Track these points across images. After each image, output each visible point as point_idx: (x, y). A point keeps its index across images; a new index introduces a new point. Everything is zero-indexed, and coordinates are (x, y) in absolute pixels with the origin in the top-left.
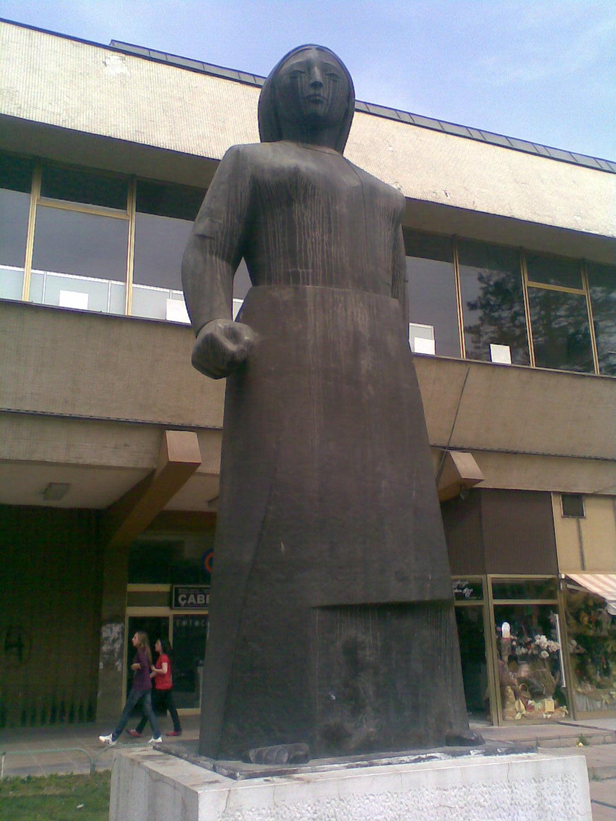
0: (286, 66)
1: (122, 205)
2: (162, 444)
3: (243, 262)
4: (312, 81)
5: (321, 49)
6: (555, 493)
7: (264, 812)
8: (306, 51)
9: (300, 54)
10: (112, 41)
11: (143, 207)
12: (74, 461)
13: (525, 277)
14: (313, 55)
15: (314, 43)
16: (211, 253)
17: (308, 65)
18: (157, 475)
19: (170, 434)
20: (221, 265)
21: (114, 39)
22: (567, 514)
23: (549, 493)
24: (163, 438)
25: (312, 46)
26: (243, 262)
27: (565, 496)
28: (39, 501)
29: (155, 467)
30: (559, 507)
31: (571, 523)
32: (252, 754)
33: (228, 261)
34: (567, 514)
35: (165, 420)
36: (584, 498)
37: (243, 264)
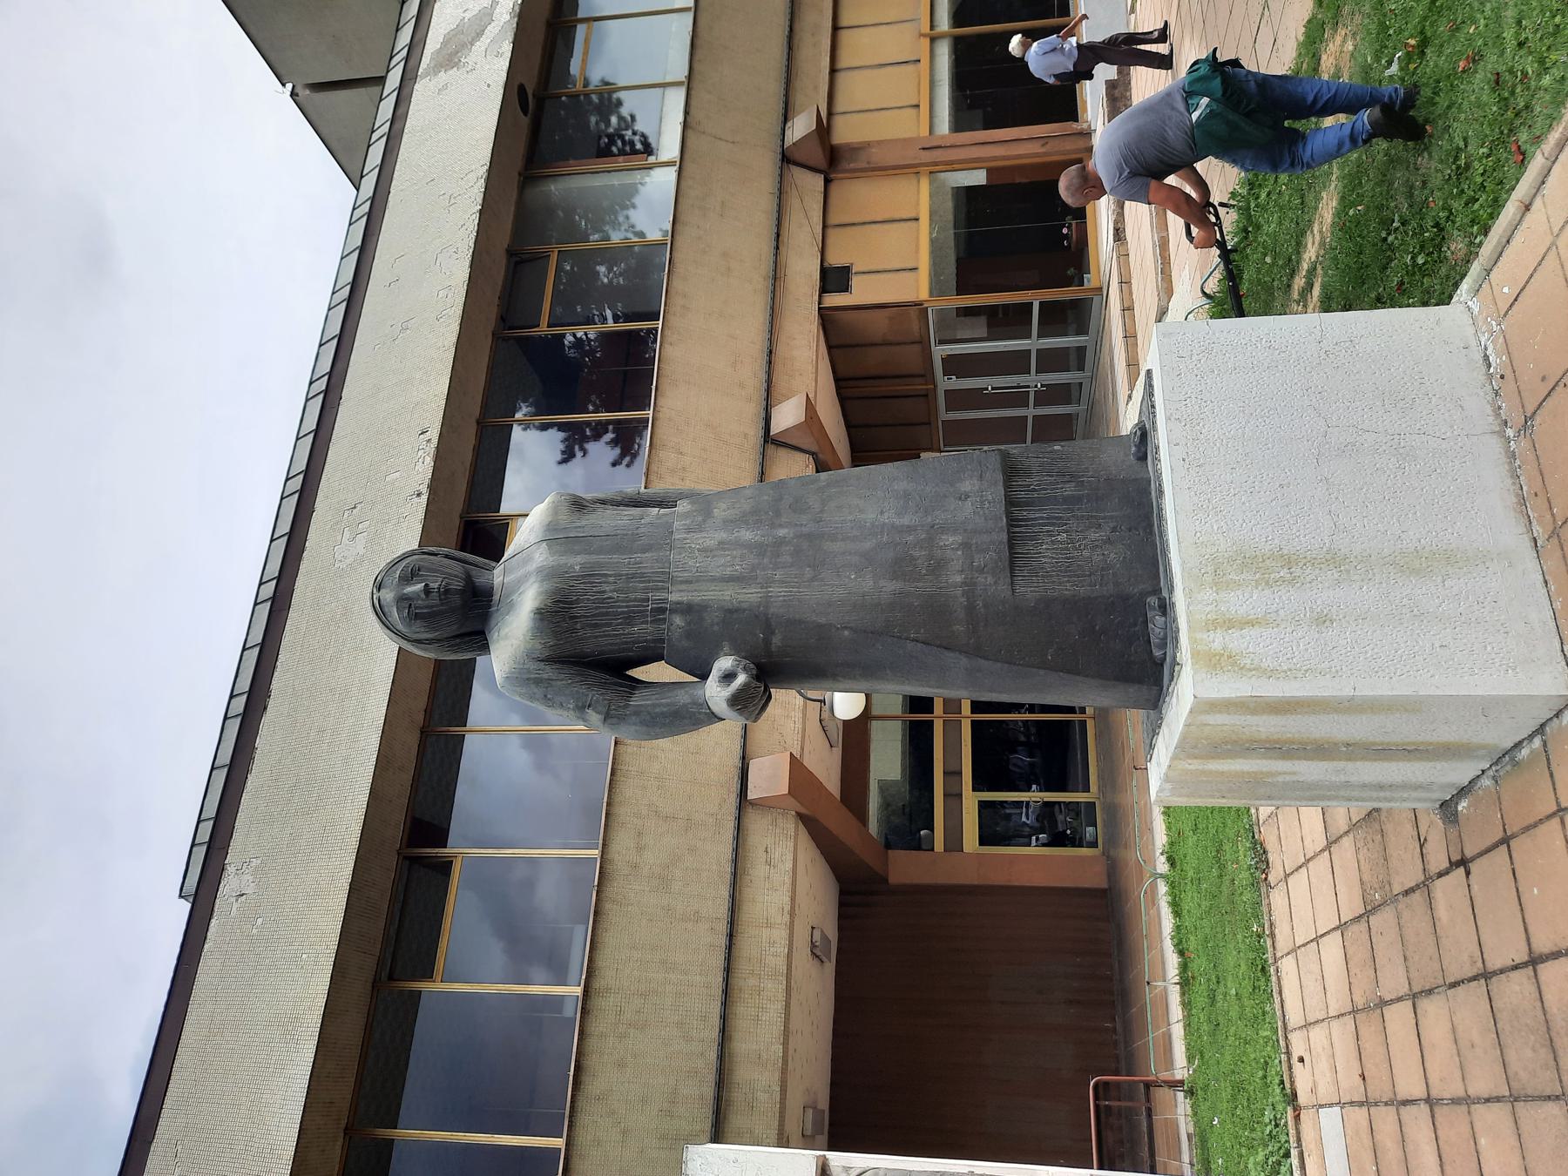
0: (400, 627)
1: (445, 867)
2: (763, 804)
3: (630, 673)
4: (423, 596)
5: (379, 586)
6: (819, 304)
7: (1211, 636)
8: (382, 602)
9: (386, 610)
10: (181, 896)
11: (441, 838)
12: (787, 918)
13: (535, 332)
14: (388, 596)
15: (369, 595)
16: (627, 706)
17: (402, 600)
18: (803, 810)
19: (751, 795)
20: (639, 700)
21: (178, 893)
22: (845, 288)
23: (819, 308)
24: (753, 803)
25: (375, 597)
26: (630, 673)
27: (824, 289)
28: (830, 967)
29: (794, 813)
30: (836, 298)
31: (856, 282)
32: (1157, 653)
33: (634, 688)
34: (845, 288)
35: (733, 800)
36: (826, 265)
37: (638, 673)
